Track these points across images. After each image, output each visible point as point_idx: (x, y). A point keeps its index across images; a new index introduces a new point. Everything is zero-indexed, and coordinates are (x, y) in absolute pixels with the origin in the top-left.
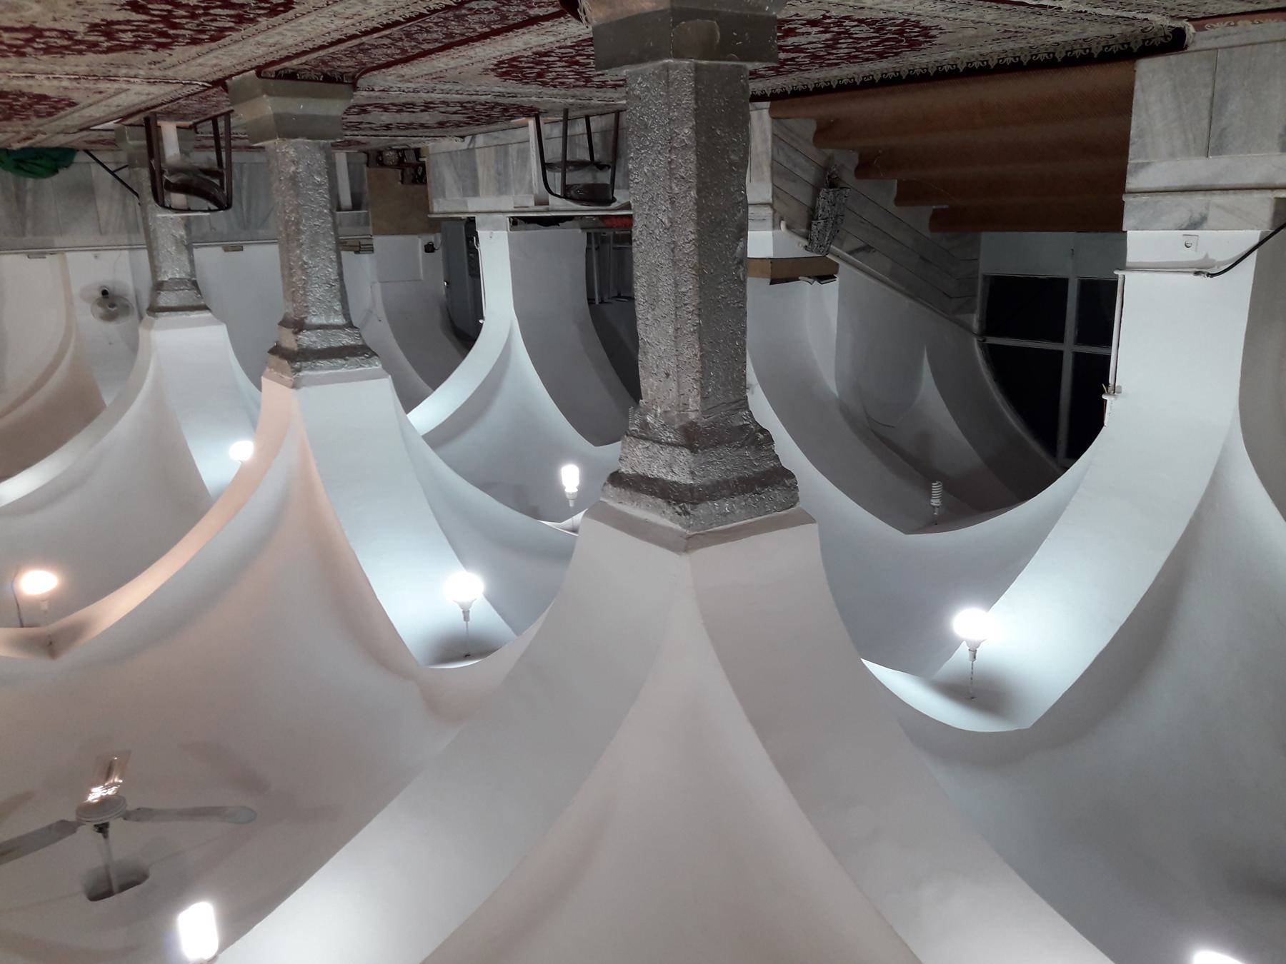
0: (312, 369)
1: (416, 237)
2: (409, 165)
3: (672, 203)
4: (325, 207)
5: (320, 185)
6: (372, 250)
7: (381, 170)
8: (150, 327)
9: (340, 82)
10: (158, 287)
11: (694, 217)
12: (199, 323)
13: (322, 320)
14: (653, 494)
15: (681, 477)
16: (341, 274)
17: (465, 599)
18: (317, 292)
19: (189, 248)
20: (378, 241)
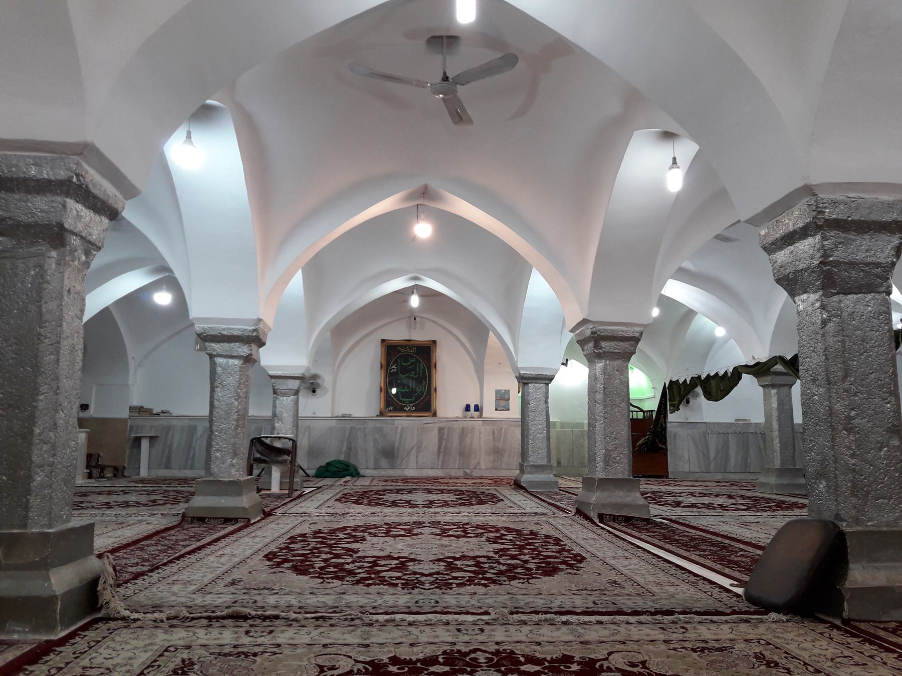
0: (245, 330)
1: (94, 416)
2: (95, 467)
3: (55, 424)
4: (216, 436)
5: (218, 451)
6: (131, 408)
7: (114, 464)
8: (308, 369)
9: (193, 518)
10: (297, 393)
11: (37, 414)
12: (279, 368)
13: (231, 361)
14: (95, 197)
15: (74, 207)
16: (212, 391)
17: (188, 147)
18: (231, 381)
19: (274, 415)
20: (125, 414)
